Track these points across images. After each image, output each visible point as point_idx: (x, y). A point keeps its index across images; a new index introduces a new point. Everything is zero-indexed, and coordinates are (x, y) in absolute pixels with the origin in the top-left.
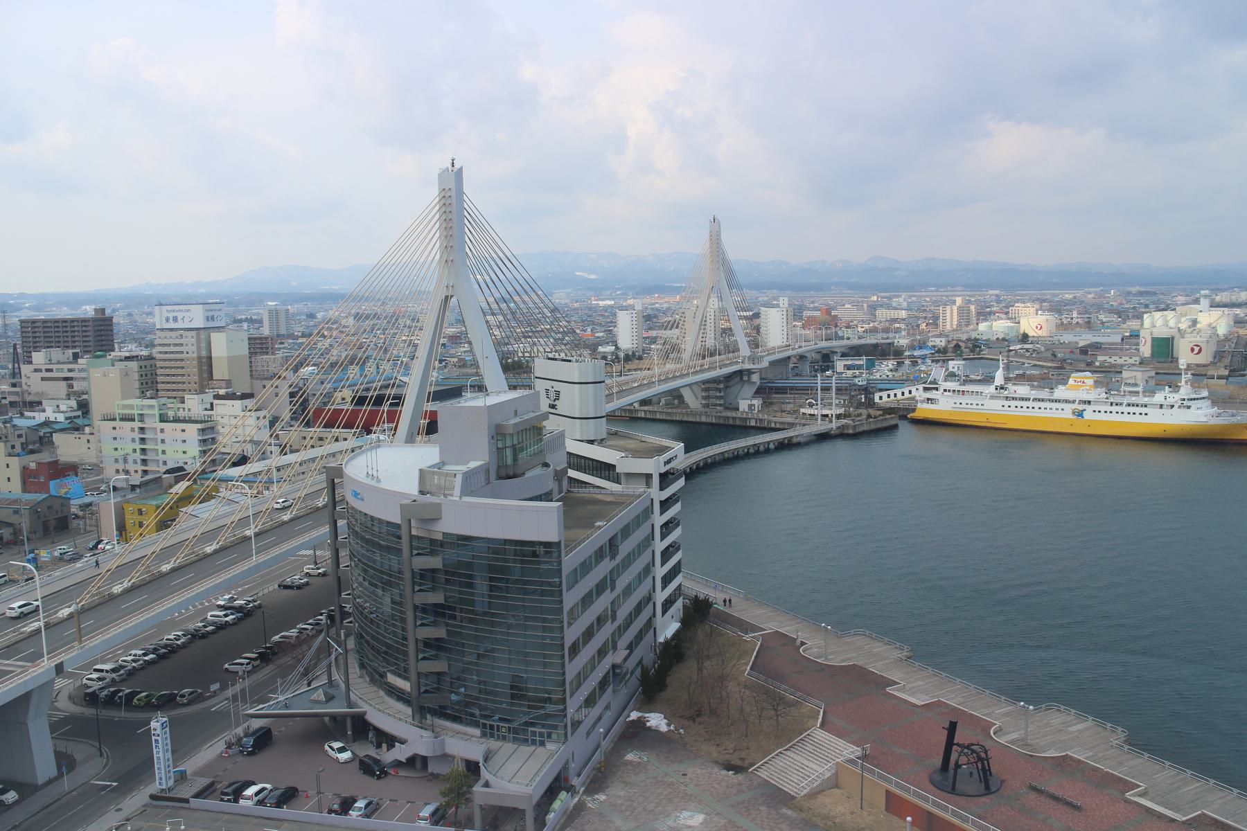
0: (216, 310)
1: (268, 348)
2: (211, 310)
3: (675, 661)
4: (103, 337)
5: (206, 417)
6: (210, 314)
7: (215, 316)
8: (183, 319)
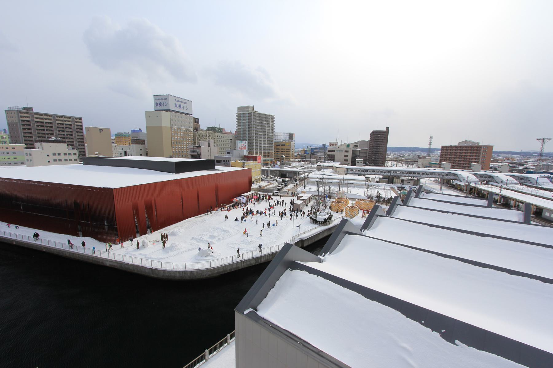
0: (162, 99)
1: (480, 156)
2: (179, 101)
3: (327, 219)
4: (379, 140)
5: (40, 147)
6: (158, 102)
7: (162, 103)
8: (183, 107)
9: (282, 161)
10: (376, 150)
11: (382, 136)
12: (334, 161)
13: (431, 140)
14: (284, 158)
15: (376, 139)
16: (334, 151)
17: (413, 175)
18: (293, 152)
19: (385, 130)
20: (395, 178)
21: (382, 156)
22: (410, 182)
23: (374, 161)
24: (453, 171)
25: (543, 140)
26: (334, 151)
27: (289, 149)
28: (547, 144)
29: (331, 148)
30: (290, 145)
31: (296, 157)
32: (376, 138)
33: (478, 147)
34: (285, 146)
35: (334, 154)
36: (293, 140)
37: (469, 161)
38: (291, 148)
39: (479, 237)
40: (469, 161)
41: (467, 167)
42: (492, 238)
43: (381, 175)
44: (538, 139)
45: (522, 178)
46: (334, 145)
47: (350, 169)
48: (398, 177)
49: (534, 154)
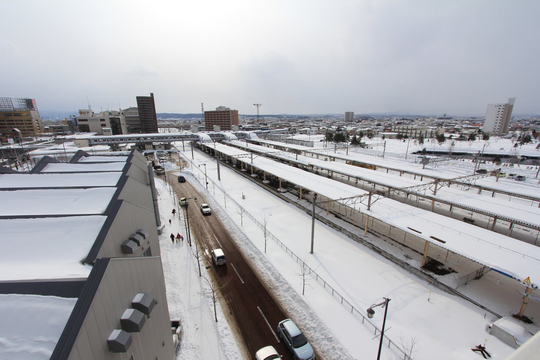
4: (145, 107)
9: (15, 136)
10: (144, 117)
11: (147, 102)
12: (90, 132)
13: (202, 107)
14: (18, 132)
15: (142, 106)
16: (86, 120)
17: (162, 140)
18: (38, 123)
19: (150, 96)
20: (146, 144)
21: (153, 123)
22: (161, 147)
23: (145, 129)
24: (222, 133)
25: (258, 105)
26: (86, 120)
27: (30, 120)
28: (260, 108)
29: (83, 117)
30: (29, 115)
31: (48, 130)
32: (142, 105)
33: (228, 112)
34: (21, 116)
35: (87, 124)
36: (33, 108)
37: (212, 124)
38: (32, 118)
39: (11, 191)
40: (212, 124)
41: (229, 129)
42: (8, 191)
43: (134, 143)
44: (254, 105)
45: (243, 135)
46: (86, 113)
47: (93, 139)
48: (151, 143)
49: (284, 117)
